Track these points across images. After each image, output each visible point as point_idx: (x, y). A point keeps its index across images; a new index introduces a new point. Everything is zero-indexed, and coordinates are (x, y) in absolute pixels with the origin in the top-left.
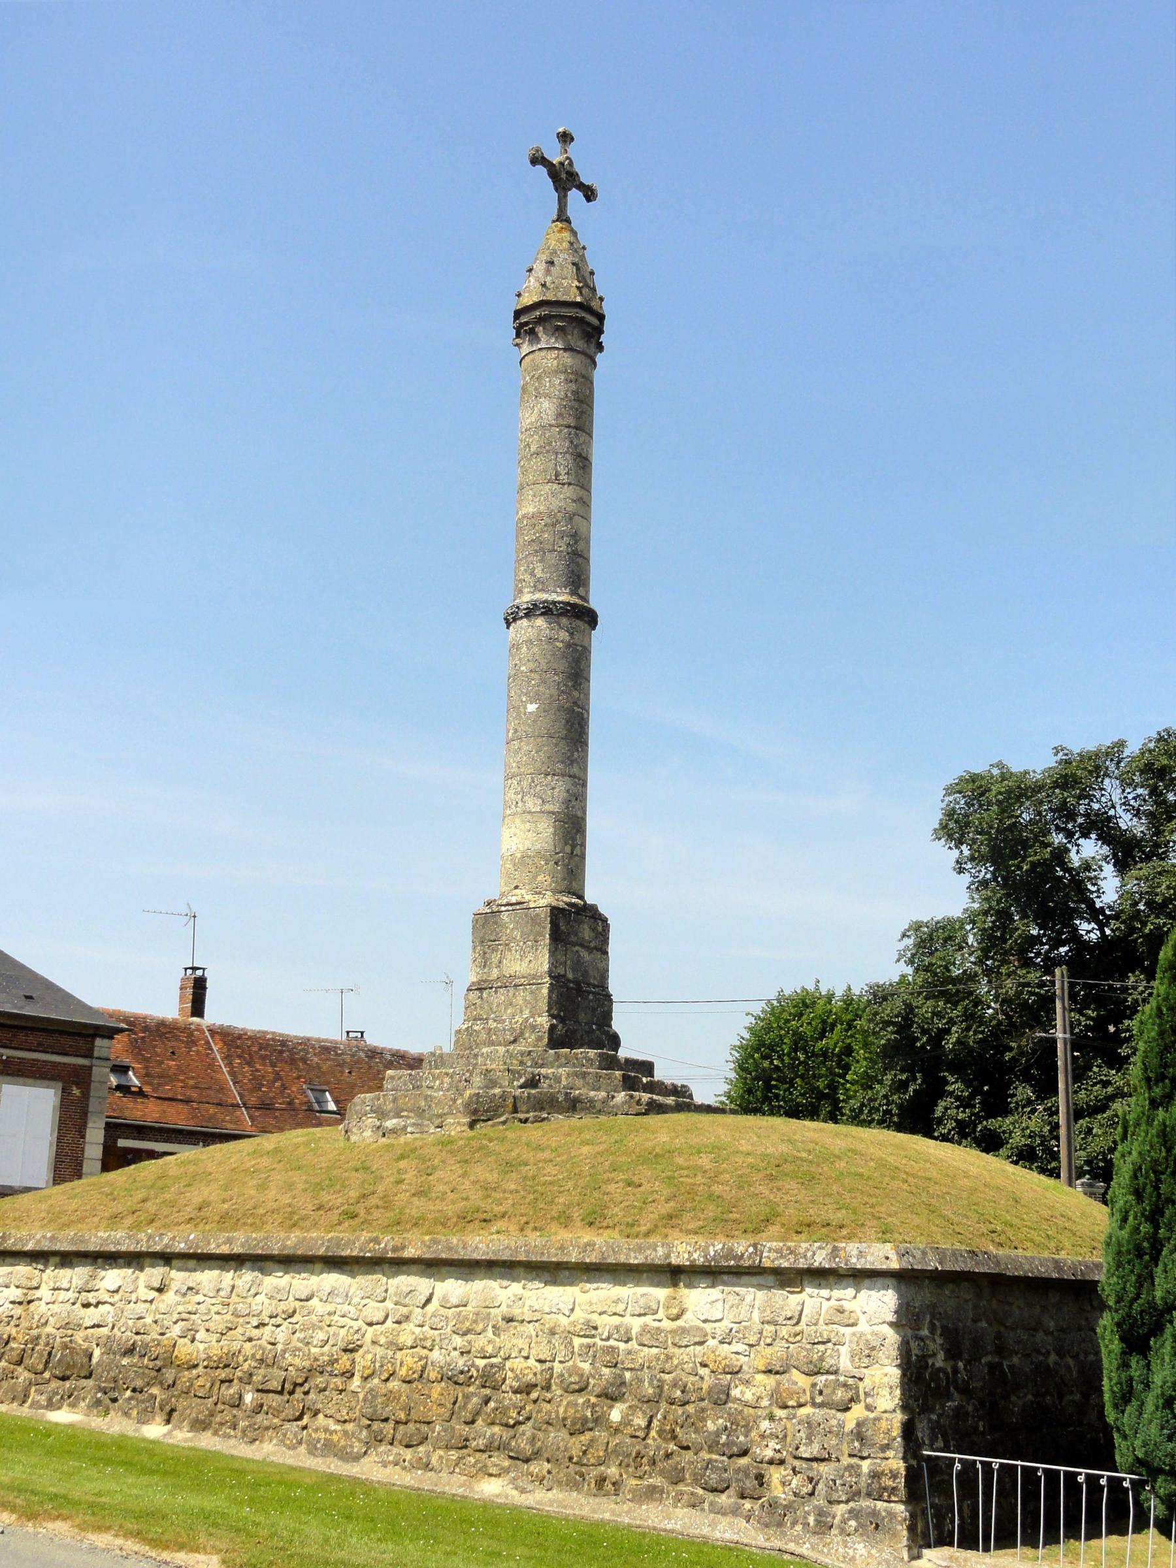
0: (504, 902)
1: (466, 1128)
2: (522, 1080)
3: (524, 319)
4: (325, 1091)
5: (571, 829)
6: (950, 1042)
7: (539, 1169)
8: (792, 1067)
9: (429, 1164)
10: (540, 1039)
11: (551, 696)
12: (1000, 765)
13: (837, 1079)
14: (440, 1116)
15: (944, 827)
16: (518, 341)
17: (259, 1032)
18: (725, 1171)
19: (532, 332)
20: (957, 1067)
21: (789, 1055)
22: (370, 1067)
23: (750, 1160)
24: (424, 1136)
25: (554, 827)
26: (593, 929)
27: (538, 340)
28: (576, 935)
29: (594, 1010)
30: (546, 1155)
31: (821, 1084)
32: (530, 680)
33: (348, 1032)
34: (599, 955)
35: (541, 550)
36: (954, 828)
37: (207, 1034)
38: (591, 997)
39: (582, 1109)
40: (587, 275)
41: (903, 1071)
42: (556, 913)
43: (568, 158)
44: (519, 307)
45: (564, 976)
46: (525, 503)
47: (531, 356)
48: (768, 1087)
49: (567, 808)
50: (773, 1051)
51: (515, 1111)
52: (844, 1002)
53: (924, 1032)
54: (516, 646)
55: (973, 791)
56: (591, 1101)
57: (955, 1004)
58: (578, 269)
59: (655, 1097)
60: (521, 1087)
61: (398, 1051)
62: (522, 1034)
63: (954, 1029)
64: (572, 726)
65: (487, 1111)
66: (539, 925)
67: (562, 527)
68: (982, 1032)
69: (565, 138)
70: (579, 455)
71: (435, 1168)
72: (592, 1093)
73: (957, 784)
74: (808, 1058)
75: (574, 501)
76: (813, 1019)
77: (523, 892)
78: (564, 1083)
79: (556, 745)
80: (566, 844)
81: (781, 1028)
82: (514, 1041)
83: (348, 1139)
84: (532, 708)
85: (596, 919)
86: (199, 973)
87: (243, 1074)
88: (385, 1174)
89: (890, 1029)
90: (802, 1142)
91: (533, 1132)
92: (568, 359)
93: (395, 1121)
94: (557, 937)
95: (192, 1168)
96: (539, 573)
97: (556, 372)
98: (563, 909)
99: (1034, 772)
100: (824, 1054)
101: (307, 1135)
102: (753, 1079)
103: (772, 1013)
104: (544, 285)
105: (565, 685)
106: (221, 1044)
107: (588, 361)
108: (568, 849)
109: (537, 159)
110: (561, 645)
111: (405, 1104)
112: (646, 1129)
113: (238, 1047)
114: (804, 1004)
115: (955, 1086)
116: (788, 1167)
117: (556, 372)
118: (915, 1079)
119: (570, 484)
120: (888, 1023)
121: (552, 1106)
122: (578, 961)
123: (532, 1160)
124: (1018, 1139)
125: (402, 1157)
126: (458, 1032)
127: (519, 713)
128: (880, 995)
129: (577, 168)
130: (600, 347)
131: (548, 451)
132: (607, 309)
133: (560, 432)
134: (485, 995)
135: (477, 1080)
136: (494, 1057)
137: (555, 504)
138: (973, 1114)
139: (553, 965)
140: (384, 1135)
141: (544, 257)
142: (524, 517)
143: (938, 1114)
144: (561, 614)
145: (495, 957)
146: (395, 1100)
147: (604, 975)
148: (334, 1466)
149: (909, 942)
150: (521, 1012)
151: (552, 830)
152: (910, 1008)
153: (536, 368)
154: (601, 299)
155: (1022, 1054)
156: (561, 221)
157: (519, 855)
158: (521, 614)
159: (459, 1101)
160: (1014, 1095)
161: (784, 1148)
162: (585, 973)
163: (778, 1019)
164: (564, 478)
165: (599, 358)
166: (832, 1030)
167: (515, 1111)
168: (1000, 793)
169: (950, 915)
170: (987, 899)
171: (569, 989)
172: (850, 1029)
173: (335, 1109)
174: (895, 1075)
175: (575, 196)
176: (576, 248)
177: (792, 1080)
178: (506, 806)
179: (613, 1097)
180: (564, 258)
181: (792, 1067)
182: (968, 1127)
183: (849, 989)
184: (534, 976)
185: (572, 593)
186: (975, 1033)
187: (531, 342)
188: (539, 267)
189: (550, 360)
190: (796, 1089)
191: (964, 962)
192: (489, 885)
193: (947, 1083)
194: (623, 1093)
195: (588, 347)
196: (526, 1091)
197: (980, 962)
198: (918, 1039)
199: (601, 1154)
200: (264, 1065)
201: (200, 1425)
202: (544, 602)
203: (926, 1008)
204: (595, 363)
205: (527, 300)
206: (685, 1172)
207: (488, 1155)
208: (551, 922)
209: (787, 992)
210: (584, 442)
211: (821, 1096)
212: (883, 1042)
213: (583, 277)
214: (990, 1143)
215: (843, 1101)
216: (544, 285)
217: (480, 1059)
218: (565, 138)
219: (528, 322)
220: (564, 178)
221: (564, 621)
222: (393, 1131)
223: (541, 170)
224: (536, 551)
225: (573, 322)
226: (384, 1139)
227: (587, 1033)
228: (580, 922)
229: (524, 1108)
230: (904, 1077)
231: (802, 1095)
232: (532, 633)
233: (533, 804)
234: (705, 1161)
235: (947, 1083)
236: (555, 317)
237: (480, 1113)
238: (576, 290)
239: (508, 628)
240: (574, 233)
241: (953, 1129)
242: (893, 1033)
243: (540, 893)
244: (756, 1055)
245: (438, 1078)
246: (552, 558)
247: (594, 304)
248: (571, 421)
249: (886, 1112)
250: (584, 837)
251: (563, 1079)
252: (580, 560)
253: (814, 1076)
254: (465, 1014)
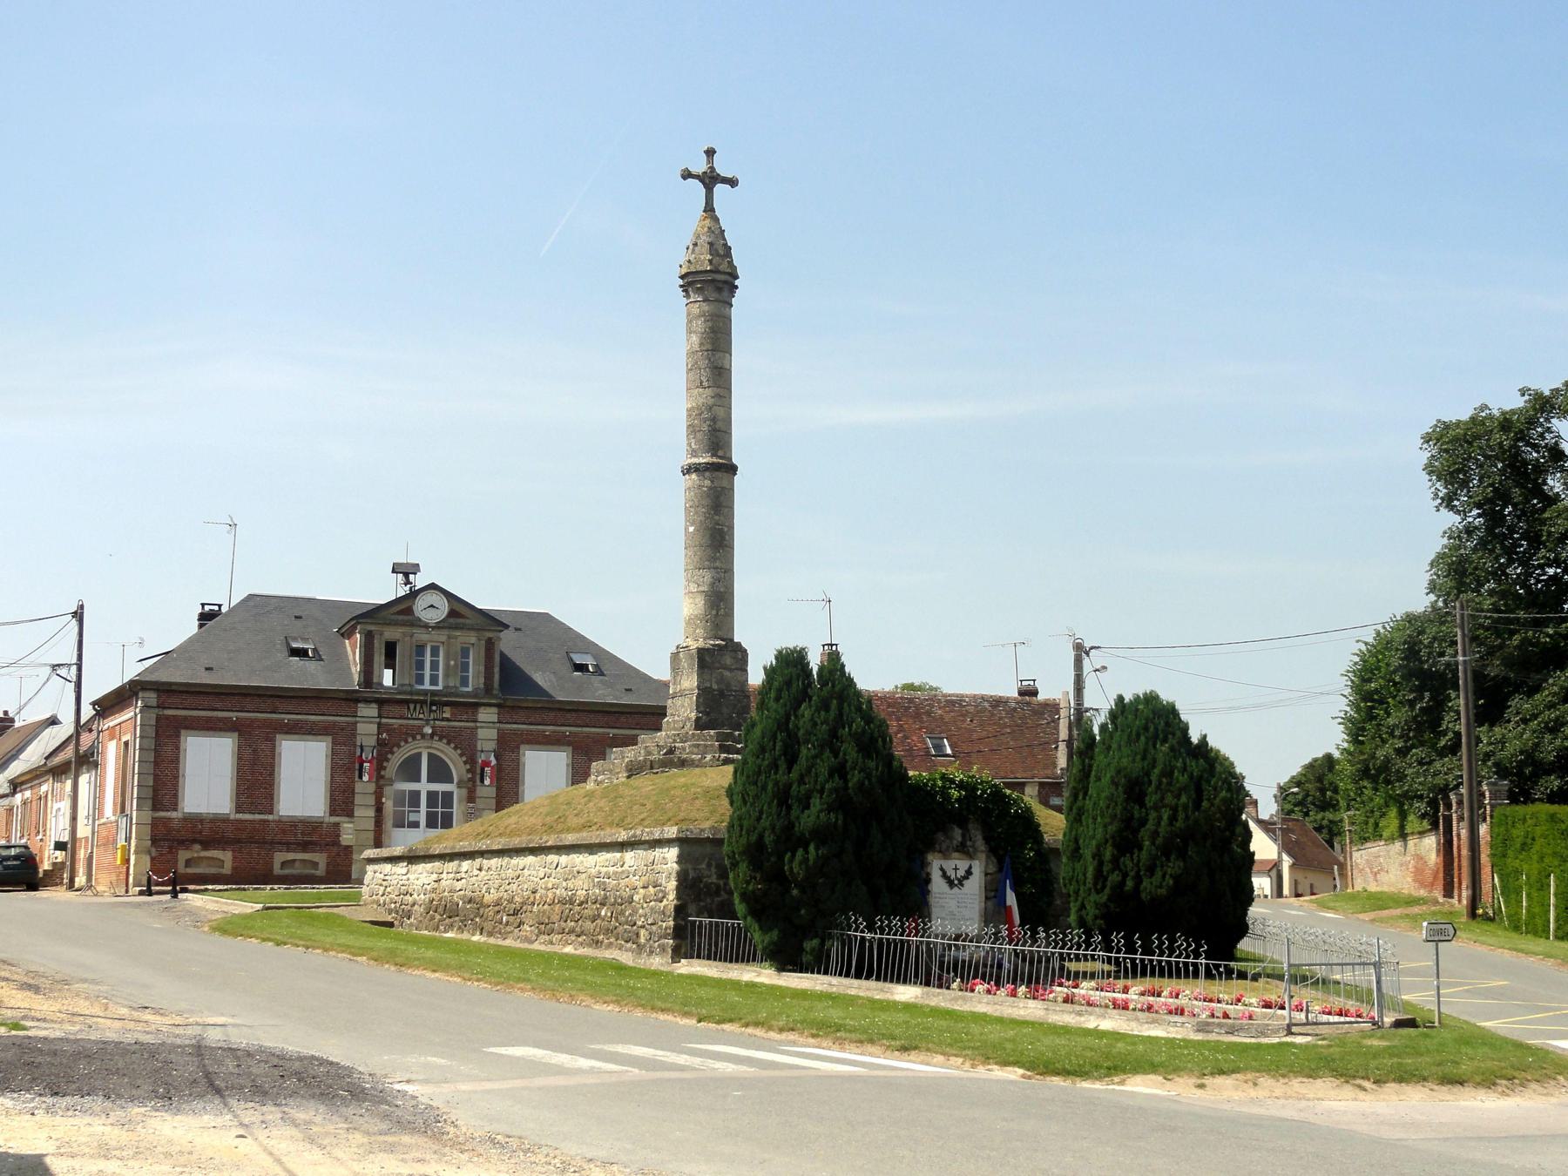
12: (1427, 439)
41: (1411, 691)
92: (705, 307)
148: (526, 945)
162: (728, 685)
201: (490, 934)
220: (710, 180)
225: (713, 281)
233: (694, 588)
240: (716, 220)
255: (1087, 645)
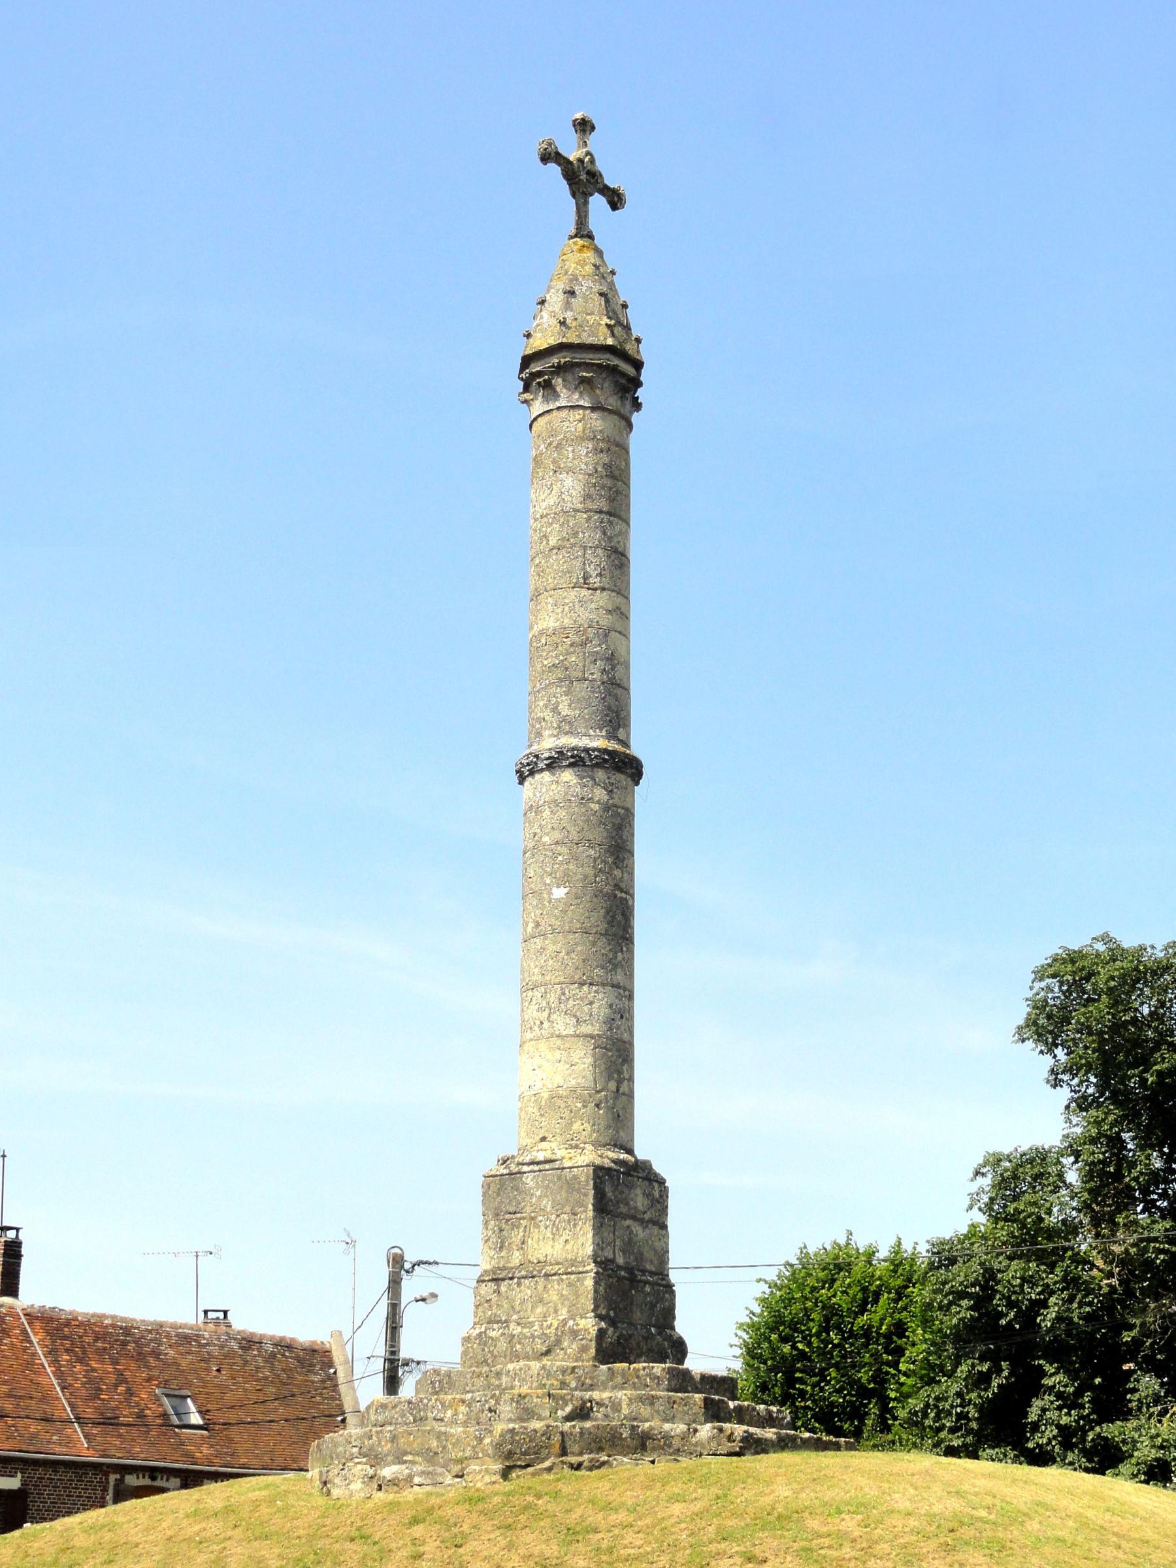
0: (527, 1160)
1: (497, 1478)
2: (568, 1409)
3: (536, 367)
4: (186, 1397)
5: (616, 1056)
6: (1047, 1319)
7: (615, 1537)
8: (823, 1353)
9: (455, 1530)
10: (584, 1349)
11: (586, 877)
12: (1105, 938)
13: (885, 1368)
14: (460, 1461)
15: (1031, 1023)
16: (527, 396)
17: (93, 1316)
18: (881, 1539)
19: (547, 385)
20: (1057, 1352)
21: (818, 1335)
22: (246, 1362)
23: (913, 1522)
24: (438, 1489)
25: (594, 1055)
26: (648, 1195)
27: (556, 396)
28: (627, 1204)
29: (653, 1306)
30: (622, 1516)
31: (864, 1376)
32: (556, 854)
33: (206, 1312)
34: (656, 1230)
35: (568, 681)
36: (1046, 1026)
37: (23, 1319)
38: (648, 1289)
39: (654, 1449)
40: (619, 309)
41: (982, 1359)
42: (601, 1174)
43: (588, 153)
44: (529, 352)
45: (613, 1261)
46: (543, 614)
47: (546, 418)
48: (790, 1381)
49: (610, 1029)
50: (796, 1330)
51: (564, 1452)
52: (892, 1262)
53: (1011, 1305)
54: (534, 809)
55: (1074, 973)
56: (667, 1437)
57: (1052, 1267)
58: (607, 301)
59: (752, 1430)
60: (568, 1418)
61: (282, 1339)
62: (558, 1342)
63: (1052, 1300)
64: (613, 917)
65: (525, 1454)
66: (578, 1191)
67: (594, 647)
68: (1090, 1304)
69: (584, 126)
70: (615, 551)
71: (465, 1536)
72: (667, 1426)
73: (1050, 966)
74: (844, 1339)
75: (609, 612)
76: (849, 1286)
77: (554, 1145)
78: (625, 1411)
79: (594, 944)
80: (610, 1078)
81: (807, 1299)
82: (547, 1352)
83: (329, 1493)
84: (560, 893)
85: (650, 1180)
86: (11, 1234)
87: (73, 1374)
88: (394, 1546)
89: (965, 1303)
90: (976, 1494)
91: (595, 1484)
92: (597, 421)
93: (395, 1468)
94: (602, 1207)
95: (108, 1536)
96: (564, 710)
97: (583, 438)
98: (610, 1169)
99: (1153, 947)
100: (867, 1332)
101: (267, 1486)
102: (769, 1370)
103: (794, 1278)
104: (563, 323)
105: (604, 862)
106: (42, 1335)
107: (624, 423)
108: (612, 1085)
109: (550, 156)
110: (596, 807)
111: (410, 1444)
112: (757, 1480)
113: (66, 1338)
114: (837, 1265)
115: (1055, 1379)
116: (967, 1533)
117: (583, 438)
118: (999, 1371)
119: (603, 589)
120: (962, 1295)
121: (613, 1445)
122: (630, 1240)
123: (603, 1525)
124: (1146, 1452)
125: (415, 1521)
126: (467, 1339)
127: (541, 900)
128: (946, 1256)
129: (600, 166)
130: (637, 405)
131: (573, 546)
132: (645, 353)
133: (589, 519)
134: (503, 1289)
135: (507, 1409)
136: (526, 1376)
137: (584, 615)
138: (1081, 1417)
139: (599, 1246)
140: (380, 1488)
141: (561, 285)
142: (542, 632)
143: (1033, 1417)
144: (597, 765)
145: (516, 1236)
146: (394, 1439)
147: (662, 1256)
149: (986, 1182)
150: (556, 1311)
151: (590, 1060)
152: (990, 1274)
153: (553, 433)
154: (638, 341)
155: (1146, 1332)
156: (582, 237)
157: (546, 1095)
158: (541, 765)
159: (487, 1441)
160: (1134, 1390)
161: (954, 1504)
162: (640, 1257)
163: (802, 1287)
164: (595, 581)
165: (635, 418)
166: (876, 1301)
167: (564, 1452)
168: (1112, 978)
169: (1039, 1144)
170: (1098, 1123)
171: (620, 1279)
172: (899, 1299)
173: (201, 1422)
174: (973, 1366)
175: (597, 202)
176: (603, 273)
177: (823, 1370)
178: (525, 1027)
179: (696, 1431)
180: (588, 287)
181: (823, 1353)
182: (1075, 1435)
183: (899, 1244)
184: (573, 1262)
185: (612, 736)
186: (1080, 1306)
187: (546, 399)
188: (555, 300)
189: (573, 423)
190: (828, 1383)
191: (1062, 1208)
192: (509, 1138)
193: (1043, 1374)
194: (709, 1426)
195: (623, 405)
196: (578, 1425)
197: (1086, 1207)
198: (1002, 1315)
199: (699, 1515)
200: (102, 1362)
202: (573, 749)
203: (1013, 1271)
204: (630, 426)
205: (540, 342)
206: (826, 1542)
207: (540, 1516)
208: (596, 1187)
209: (812, 1250)
210: (620, 533)
211: (864, 1393)
212: (955, 1321)
213: (614, 312)
214: (1105, 1459)
215: (895, 1399)
216: (563, 323)
217: (504, 1379)
218: (584, 126)
219: (540, 372)
220: (583, 180)
221: (600, 774)
222: (394, 1482)
223: (554, 169)
224: (560, 680)
225: (603, 371)
226: (381, 1494)
227: (646, 1339)
228: (631, 1187)
229: (576, 1448)
230: (985, 1367)
231: (839, 1391)
232: (556, 792)
233: (564, 1024)
234: (850, 1524)
235: (1043, 1374)
236: (579, 365)
237: (516, 1458)
238: (606, 330)
239: (521, 782)
240: (599, 253)
241: (1055, 1437)
242: (968, 1309)
243: (577, 1147)
244: (774, 1337)
245: (450, 1406)
246: (581, 689)
247: (630, 347)
248: (603, 505)
249: (960, 1416)
250: (632, 1068)
251: (624, 1406)
252: (619, 691)
253: (853, 1366)
254: (476, 1313)
255: (410, 1257)
